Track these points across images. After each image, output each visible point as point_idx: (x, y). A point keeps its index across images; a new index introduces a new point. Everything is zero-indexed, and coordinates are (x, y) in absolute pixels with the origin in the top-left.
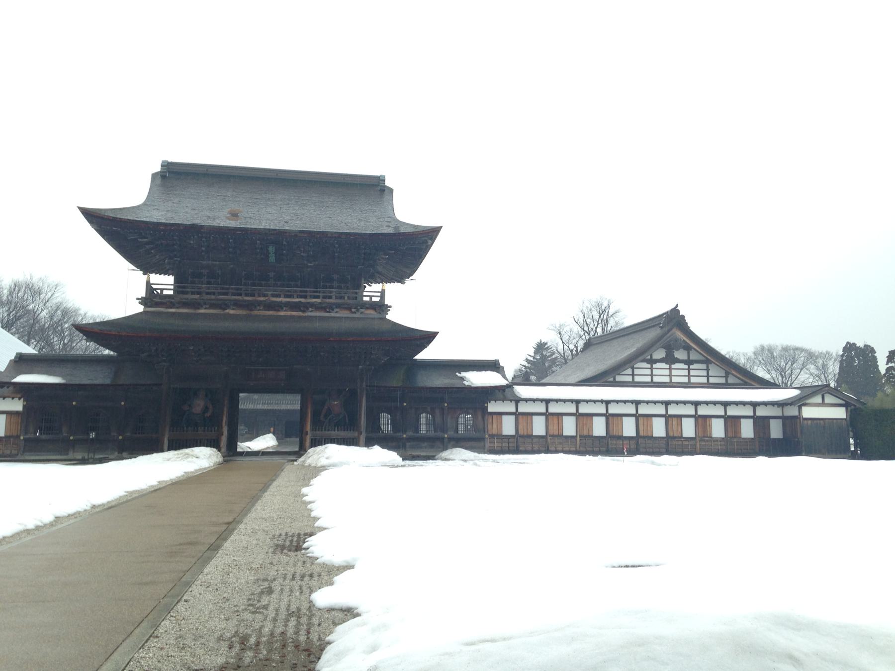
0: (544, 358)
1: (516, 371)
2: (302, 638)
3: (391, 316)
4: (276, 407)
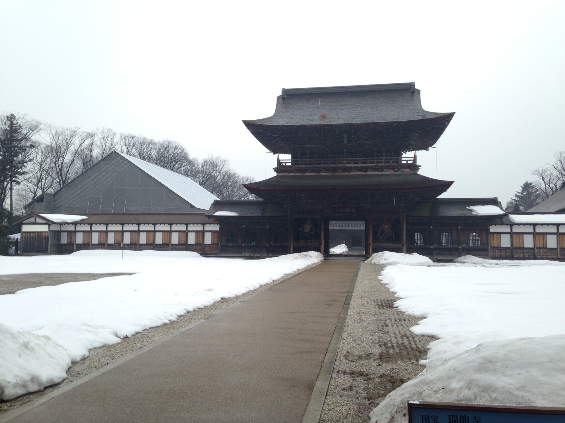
0: (530, 194)
1: (508, 204)
2: (414, 346)
3: (420, 172)
4: (346, 228)
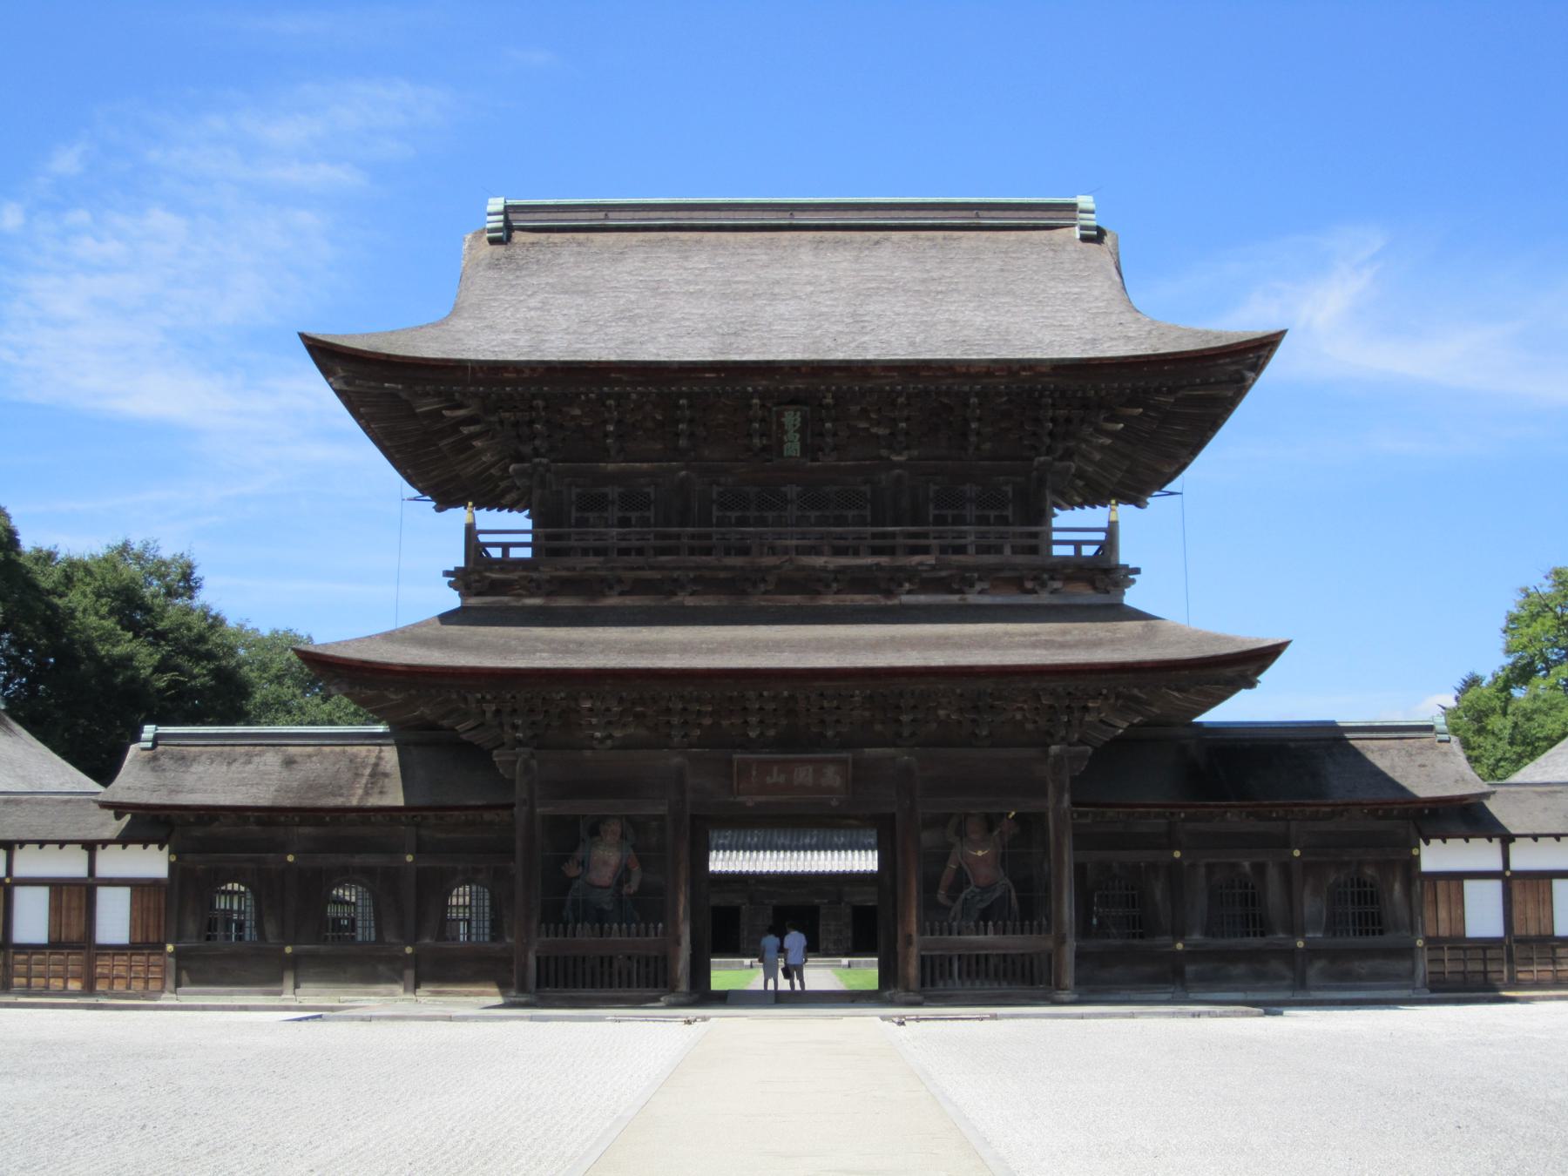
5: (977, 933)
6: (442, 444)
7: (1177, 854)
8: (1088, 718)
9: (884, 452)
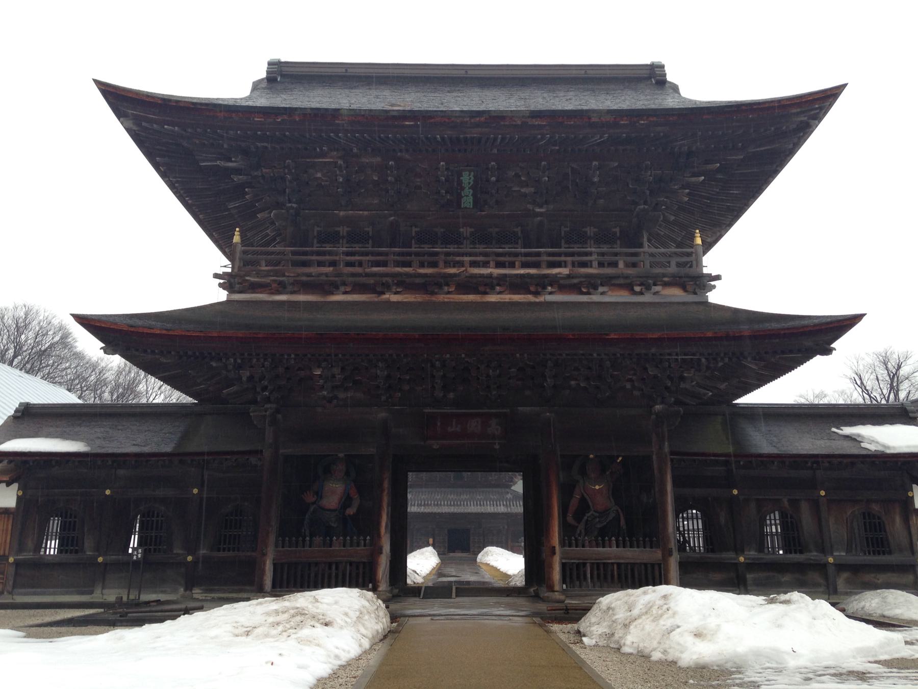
3: (717, 296)
4: (435, 510)
5: (604, 547)
6: (231, 205)
7: (735, 492)
8: (682, 385)
9: (530, 207)
